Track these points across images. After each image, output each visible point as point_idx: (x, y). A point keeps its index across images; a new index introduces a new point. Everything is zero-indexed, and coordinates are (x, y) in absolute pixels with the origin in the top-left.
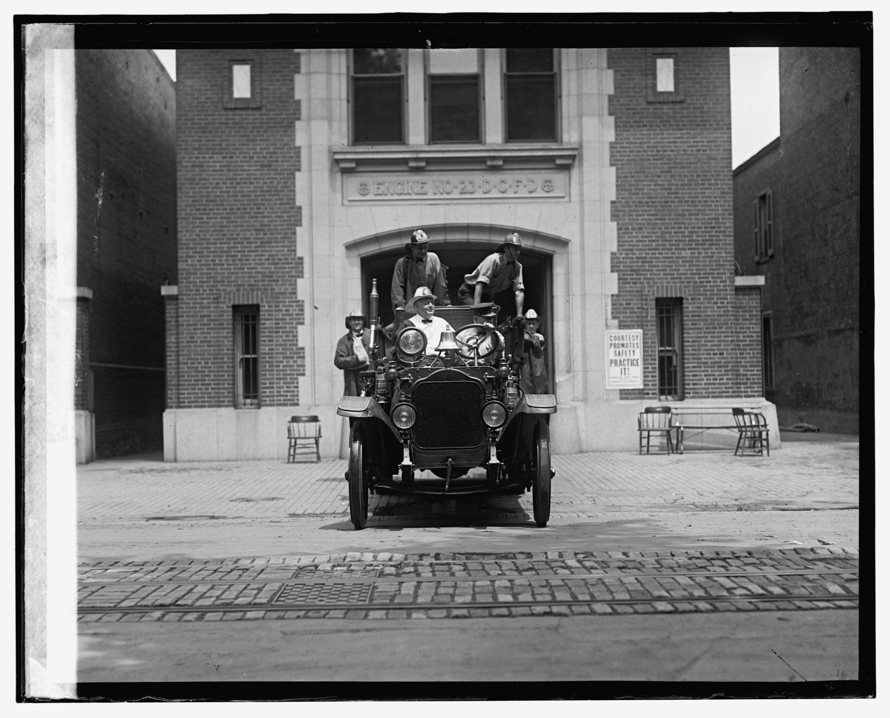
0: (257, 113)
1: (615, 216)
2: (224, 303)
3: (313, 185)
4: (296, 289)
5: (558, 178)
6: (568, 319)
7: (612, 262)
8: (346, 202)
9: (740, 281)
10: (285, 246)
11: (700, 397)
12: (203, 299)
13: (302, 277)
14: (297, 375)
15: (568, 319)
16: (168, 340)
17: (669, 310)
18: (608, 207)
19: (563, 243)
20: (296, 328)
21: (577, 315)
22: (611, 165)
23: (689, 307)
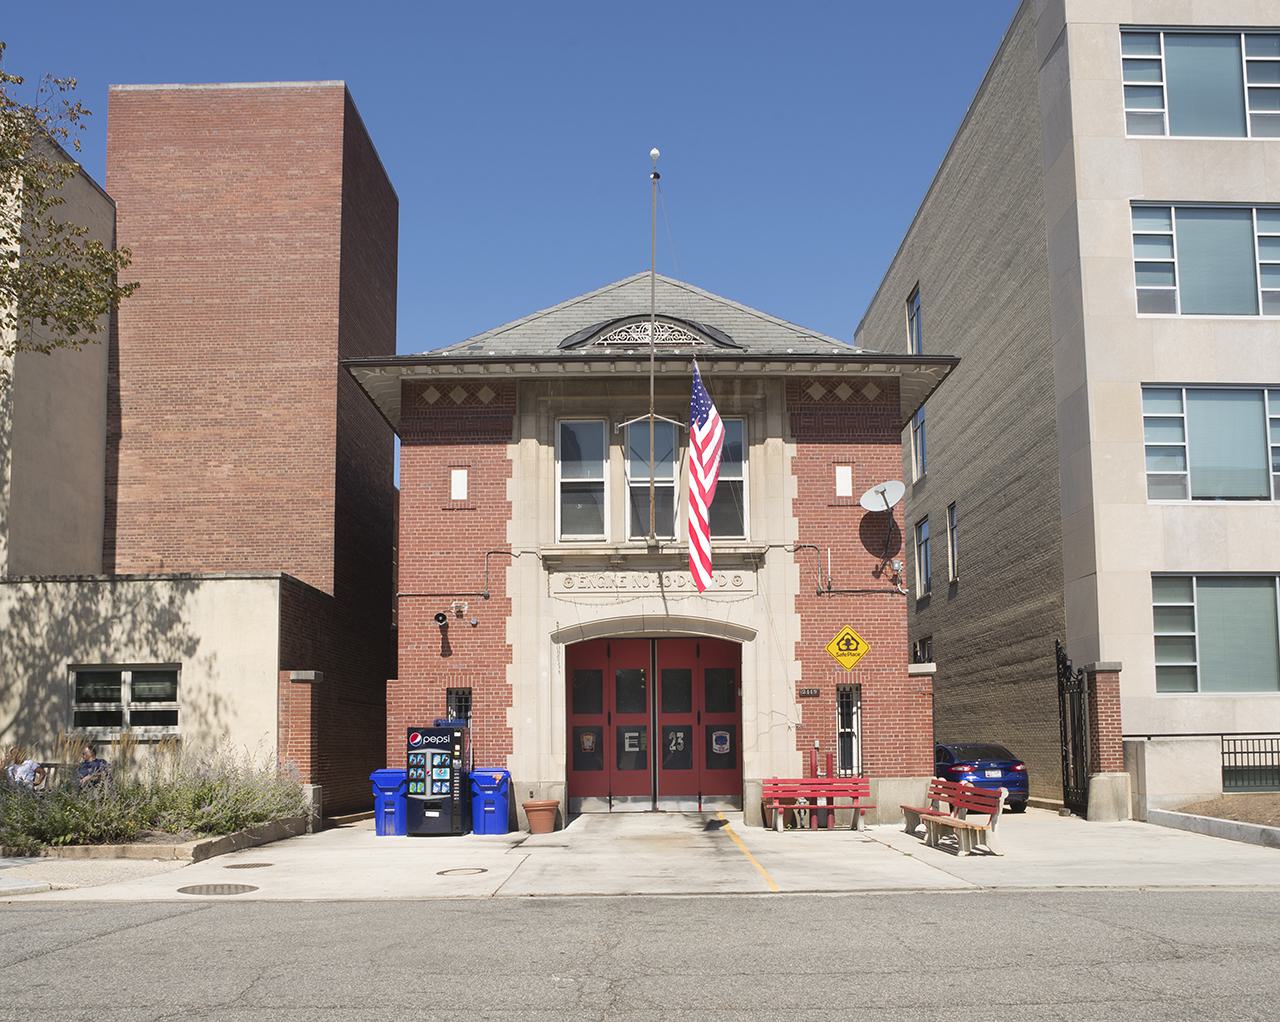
0: (473, 512)
1: (798, 609)
2: (440, 686)
3: (522, 579)
4: (505, 674)
5: (747, 575)
6: (480, 840)
7: (796, 651)
8: (552, 594)
9: (914, 668)
10: (495, 635)
11: (877, 777)
12: (421, 682)
13: (796, 682)
14: (506, 753)
15: (480, 840)
16: (388, 719)
17: (848, 698)
18: (793, 600)
19: (751, 635)
20: (505, 709)
21: (487, 844)
22: (794, 516)
23: (867, 693)
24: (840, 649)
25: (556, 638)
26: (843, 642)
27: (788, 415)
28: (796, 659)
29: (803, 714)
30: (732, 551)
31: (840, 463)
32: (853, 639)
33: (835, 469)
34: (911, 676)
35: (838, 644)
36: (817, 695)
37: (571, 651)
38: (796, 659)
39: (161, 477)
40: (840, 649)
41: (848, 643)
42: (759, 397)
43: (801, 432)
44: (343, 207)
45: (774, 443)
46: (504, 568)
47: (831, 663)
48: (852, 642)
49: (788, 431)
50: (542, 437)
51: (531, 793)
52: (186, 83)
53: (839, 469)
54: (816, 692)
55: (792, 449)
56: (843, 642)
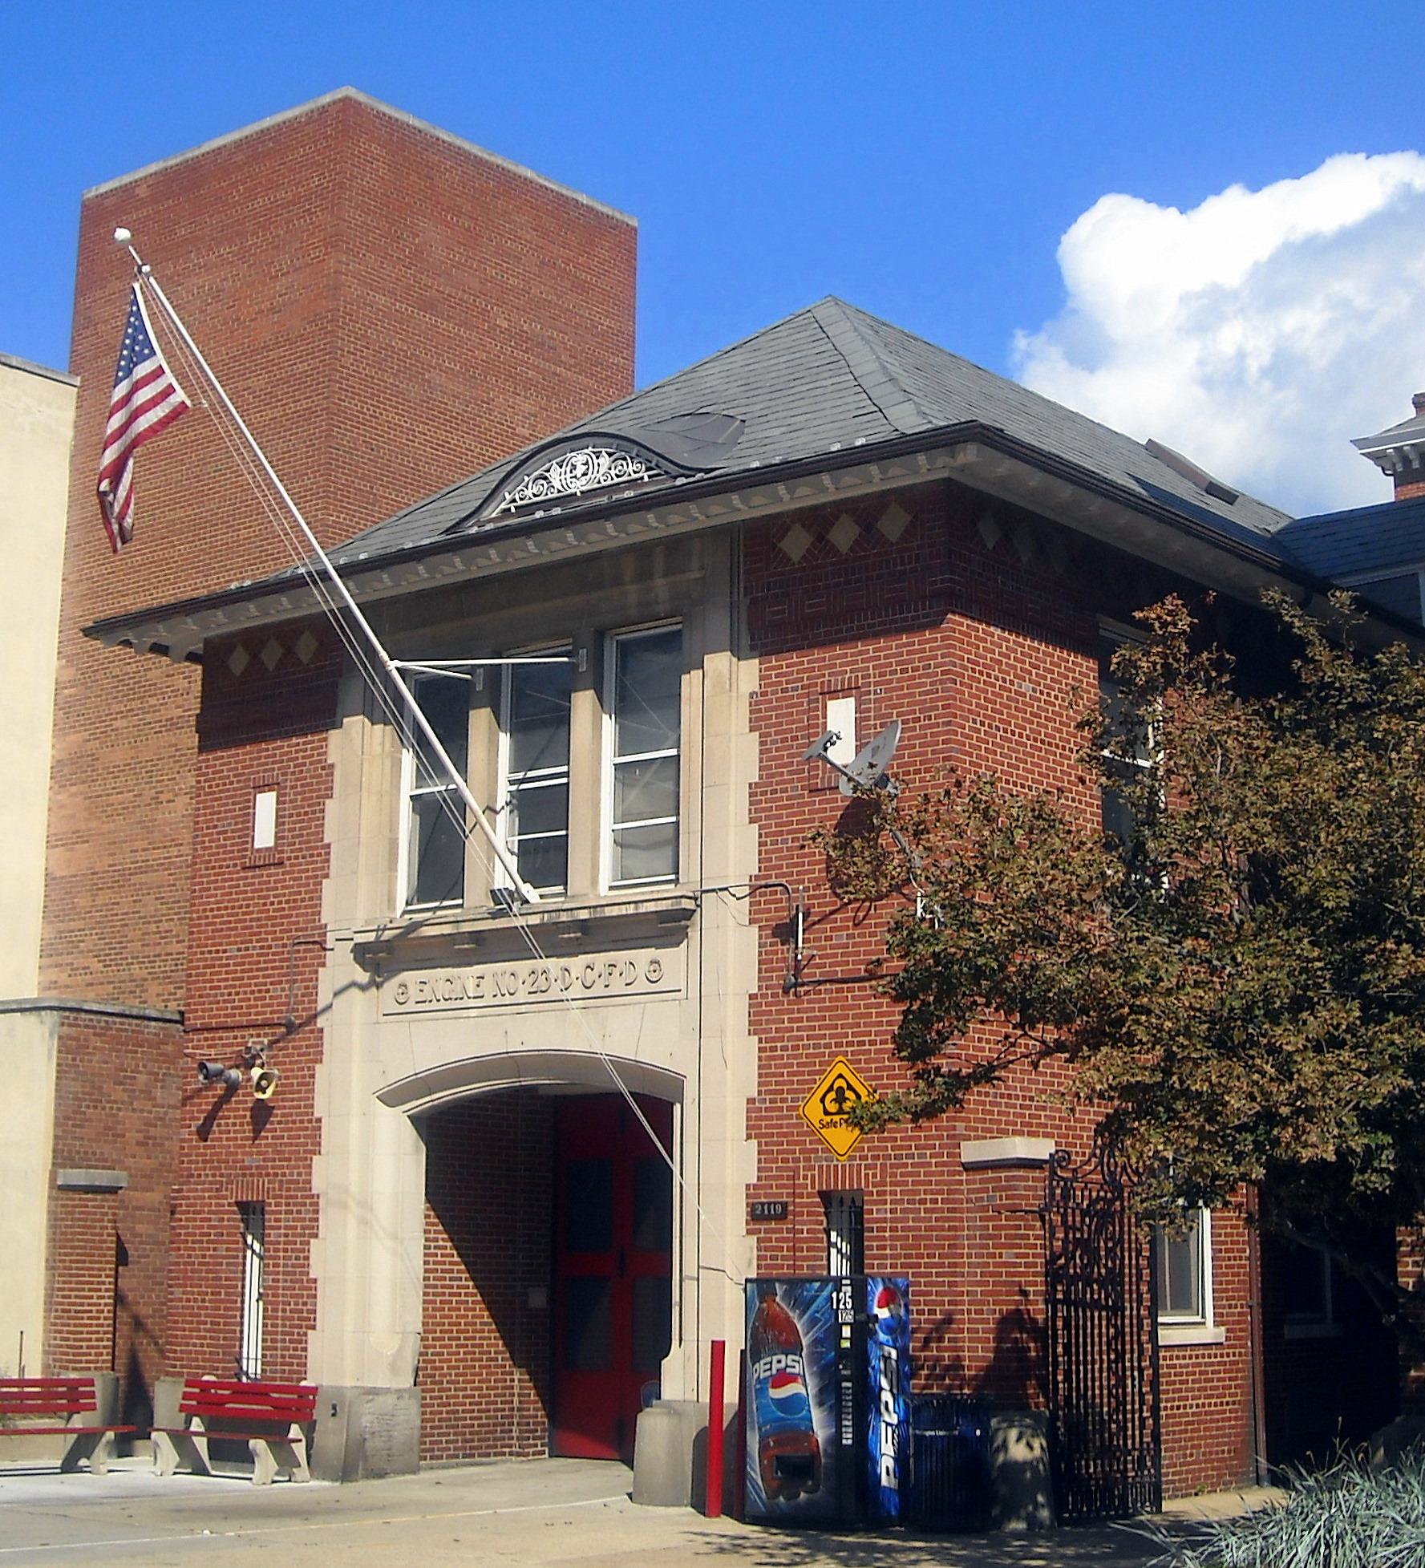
14: (308, 1327)
24: (826, 1113)
25: (392, 1098)
26: (832, 1095)
27: (745, 602)
28: (749, 1137)
29: (759, 1258)
30: (631, 910)
31: (834, 694)
32: (850, 1087)
33: (825, 707)
34: (970, 1168)
35: (822, 1100)
36: (782, 1217)
37: (430, 1125)
38: (749, 1137)
39: (105, 828)
40: (826, 1113)
41: (840, 1099)
42: (696, 575)
43: (764, 636)
44: (1085, 209)
45: (718, 662)
46: (316, 972)
47: (811, 1142)
48: (849, 1094)
49: (745, 641)
50: (376, 716)
51: (334, 1407)
52: (458, 134)
53: (832, 705)
54: (779, 1208)
55: (748, 673)
56: (832, 1095)
